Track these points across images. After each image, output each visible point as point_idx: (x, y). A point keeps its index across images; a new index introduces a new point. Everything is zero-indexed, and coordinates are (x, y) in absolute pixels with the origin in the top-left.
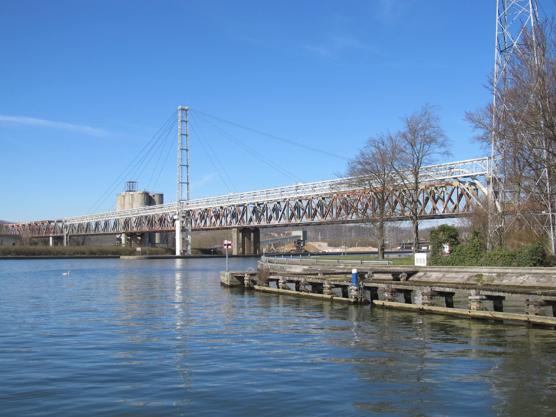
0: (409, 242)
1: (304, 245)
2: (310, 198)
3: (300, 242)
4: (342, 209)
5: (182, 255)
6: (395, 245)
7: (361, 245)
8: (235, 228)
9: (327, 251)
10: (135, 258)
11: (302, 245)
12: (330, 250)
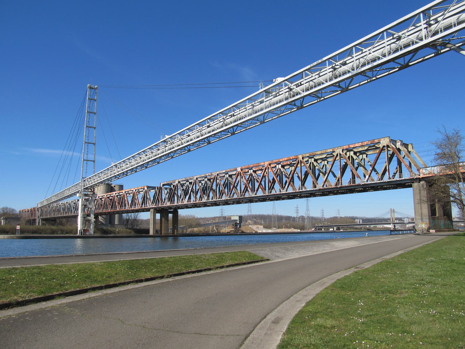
0: (320, 225)
1: (240, 227)
2: (215, 175)
3: (237, 224)
7: (287, 227)
8: (152, 208)
10: (5, 238)
11: (238, 227)
12: (265, 231)
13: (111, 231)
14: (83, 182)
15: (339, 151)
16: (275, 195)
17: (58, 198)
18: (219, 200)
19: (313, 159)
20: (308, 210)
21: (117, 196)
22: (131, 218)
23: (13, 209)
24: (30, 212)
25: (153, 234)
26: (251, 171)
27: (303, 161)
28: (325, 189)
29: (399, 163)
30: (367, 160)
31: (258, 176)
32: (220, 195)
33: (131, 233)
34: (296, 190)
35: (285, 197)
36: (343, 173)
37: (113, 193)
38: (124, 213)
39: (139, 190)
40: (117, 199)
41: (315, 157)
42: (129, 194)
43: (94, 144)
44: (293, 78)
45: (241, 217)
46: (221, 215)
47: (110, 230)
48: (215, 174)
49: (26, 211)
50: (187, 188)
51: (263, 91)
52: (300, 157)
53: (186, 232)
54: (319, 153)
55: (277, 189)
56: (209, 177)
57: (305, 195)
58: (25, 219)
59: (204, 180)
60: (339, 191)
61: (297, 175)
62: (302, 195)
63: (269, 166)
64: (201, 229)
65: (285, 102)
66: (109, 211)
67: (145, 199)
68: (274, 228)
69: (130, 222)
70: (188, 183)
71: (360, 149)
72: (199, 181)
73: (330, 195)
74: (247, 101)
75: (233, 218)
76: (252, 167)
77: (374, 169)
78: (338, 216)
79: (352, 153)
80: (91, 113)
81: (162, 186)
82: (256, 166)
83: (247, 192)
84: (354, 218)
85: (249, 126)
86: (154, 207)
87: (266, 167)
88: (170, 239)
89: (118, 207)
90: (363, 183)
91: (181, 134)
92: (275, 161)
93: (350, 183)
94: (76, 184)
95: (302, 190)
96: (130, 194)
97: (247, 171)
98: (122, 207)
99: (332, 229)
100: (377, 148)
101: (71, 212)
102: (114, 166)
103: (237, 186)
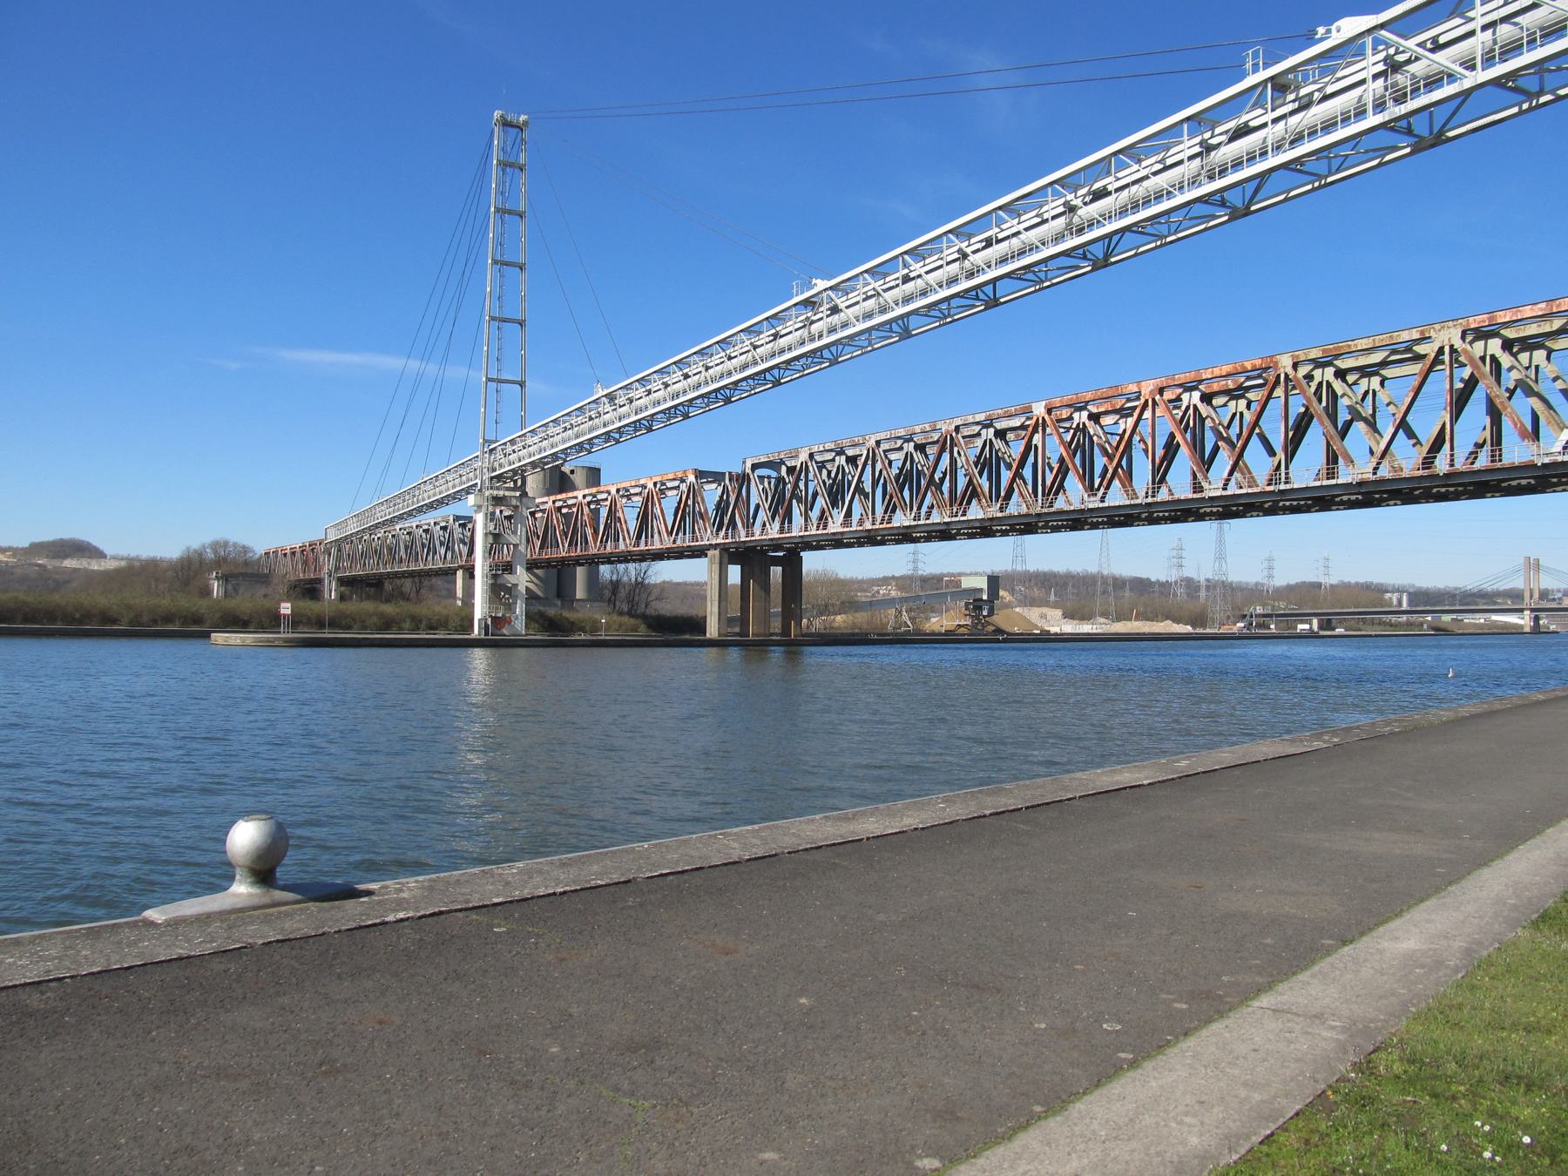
1: (991, 612)
2: (948, 431)
3: (979, 604)
4: (1068, 470)
5: (486, 634)
6: (1228, 617)
7: (1143, 616)
8: (715, 546)
9: (1054, 630)
10: (248, 642)
11: (985, 613)
12: (1069, 627)
13: (573, 623)
14: (487, 455)
15: (1449, 336)
16: (1168, 502)
17: (398, 510)
18: (881, 526)
19: (1330, 371)
20: (1221, 557)
21: (589, 504)
22: (625, 579)
23: (244, 547)
24: (298, 555)
25: (720, 635)
26: (1081, 417)
27: (1295, 376)
28: (1383, 481)
29: (1495, 414)
30: (1383, 397)
31: (1106, 433)
32: (886, 512)
33: (636, 631)
34: (1137, 498)
35: (1100, 520)
36: (1293, 444)
37: (575, 493)
38: (603, 563)
39: (665, 484)
40: (557, 519)
41: (1337, 363)
42: (629, 497)
43: (521, 323)
44: (1420, 13)
45: (994, 581)
46: (910, 573)
47: (567, 619)
48: (946, 427)
49: (285, 555)
50: (840, 476)
51: (1266, 81)
52: (1286, 362)
53: (808, 627)
54: (1363, 344)
55: (1075, 495)
56: (919, 439)
57: (1295, 503)
58: (285, 581)
59: (901, 448)
60: (1435, 490)
61: (1142, 446)
62: (1155, 515)
63: (1157, 398)
64: (860, 619)
65: (1372, 120)
66: (564, 554)
67: (686, 514)
68: (1102, 620)
69: (622, 591)
70: (843, 458)
71: (1532, 330)
72: (816, 462)
73: (1252, 516)
74: (1185, 126)
75: (967, 583)
76: (1087, 402)
77: (1403, 425)
78: (1322, 579)
79: (1495, 346)
80: (510, 212)
81: (748, 471)
82: (1104, 396)
83: (974, 502)
84: (1381, 589)
85: (1176, 232)
86: (723, 541)
87: (1147, 401)
88: (776, 654)
89: (563, 546)
90: (1547, 460)
91: (878, 273)
92: (1180, 378)
93: (1470, 461)
94: (463, 464)
95: (1288, 487)
96: (629, 499)
97: (1064, 417)
98: (577, 544)
99: (1307, 626)
100: (1419, 358)
101: (417, 560)
102: (604, 398)
103: (942, 480)
